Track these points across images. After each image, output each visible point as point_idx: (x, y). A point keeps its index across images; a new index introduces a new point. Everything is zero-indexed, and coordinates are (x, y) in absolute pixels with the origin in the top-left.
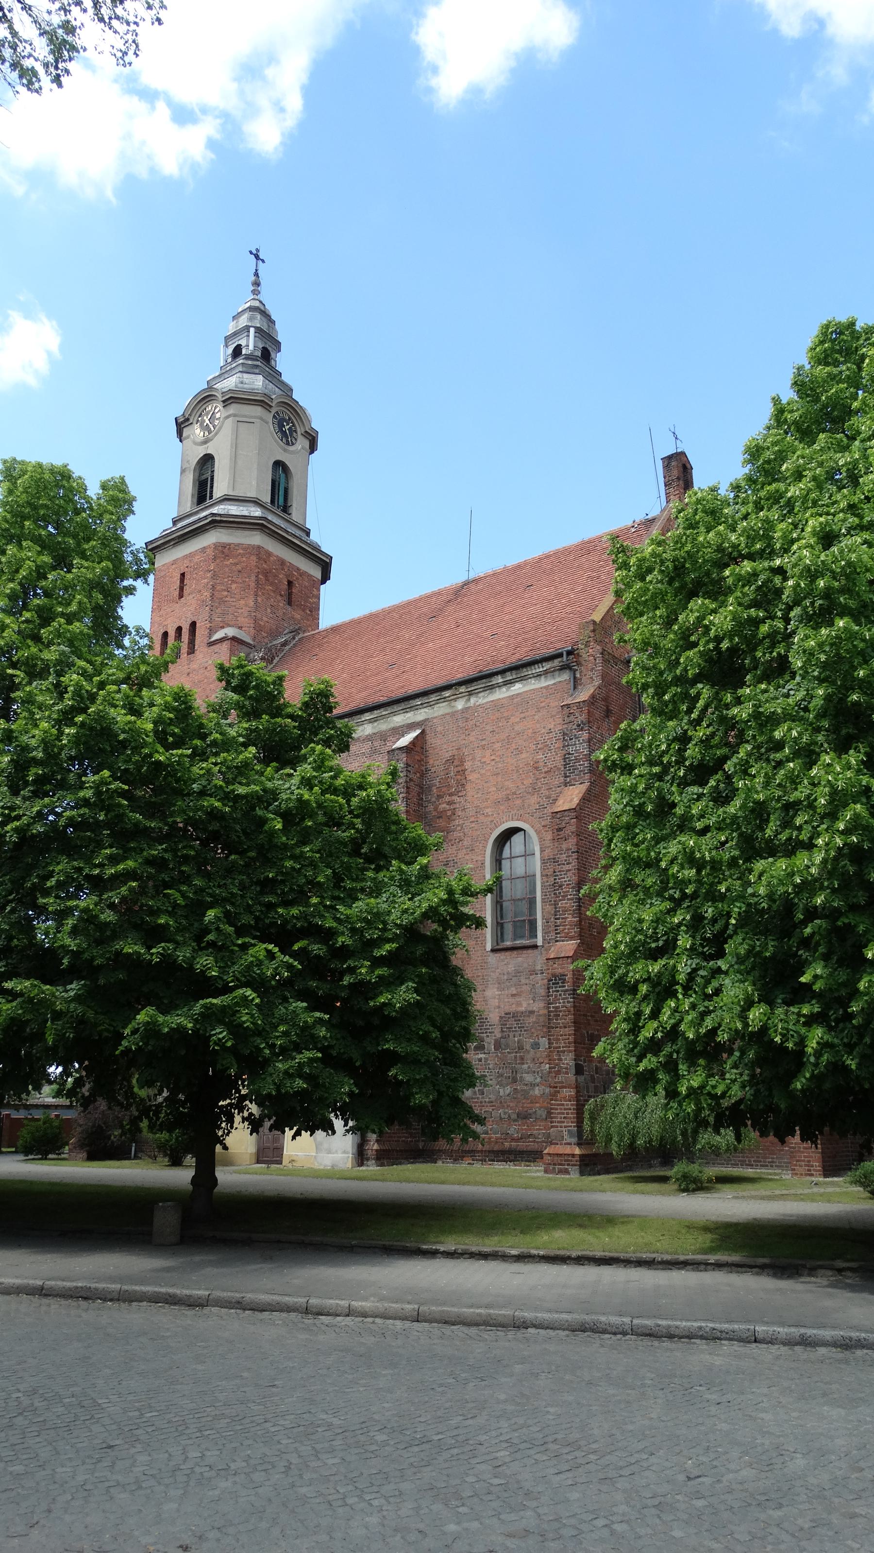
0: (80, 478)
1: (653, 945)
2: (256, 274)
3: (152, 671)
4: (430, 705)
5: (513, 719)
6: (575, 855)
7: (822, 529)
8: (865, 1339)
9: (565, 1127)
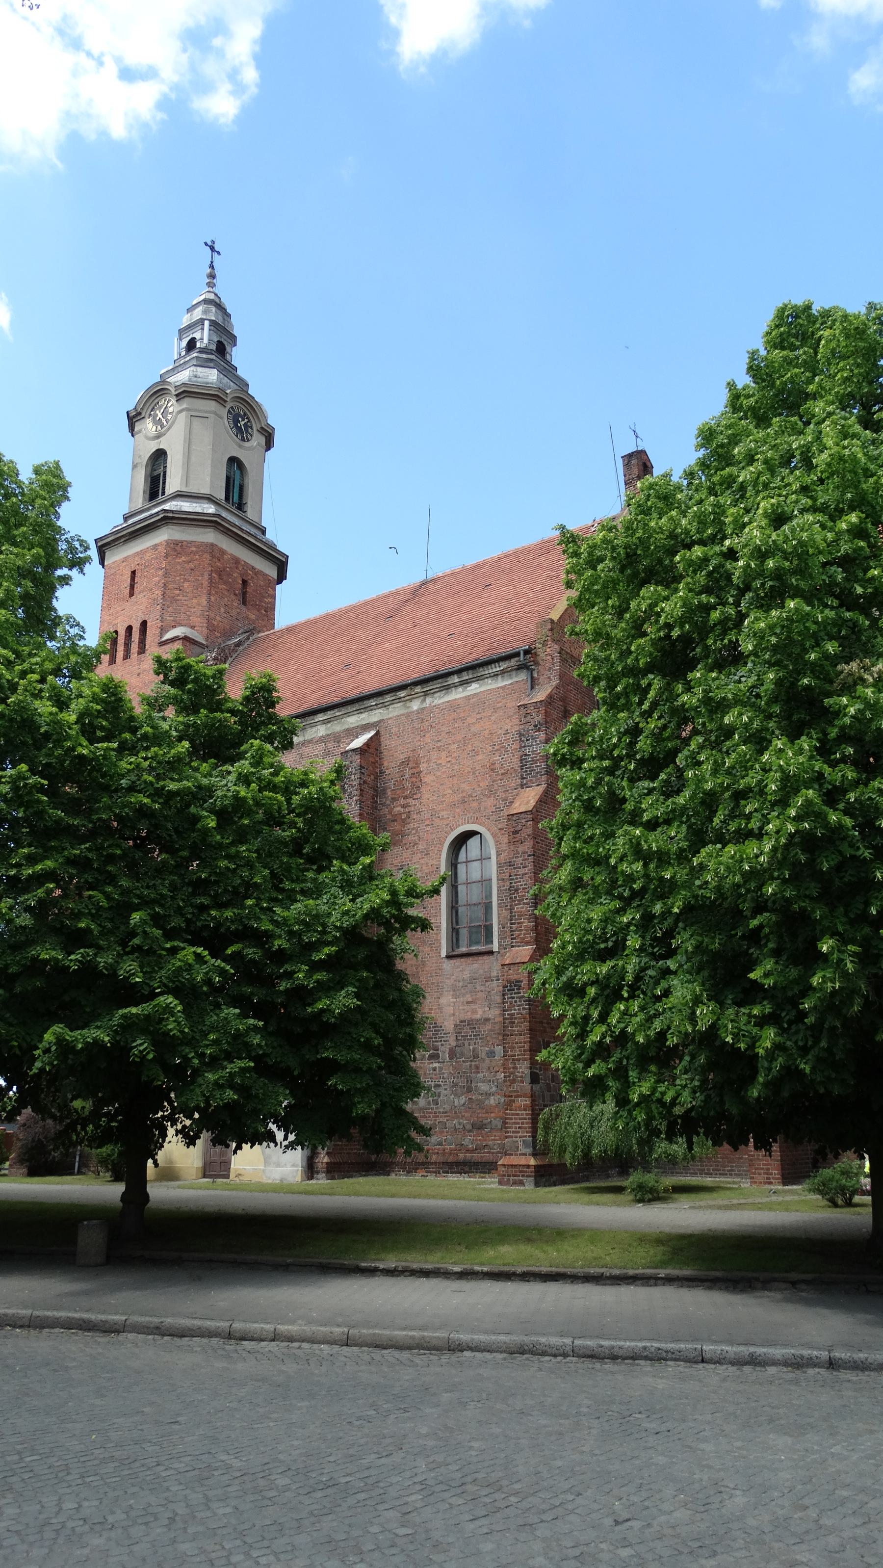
0: (12, 462)
1: (602, 946)
2: (212, 266)
3: (83, 662)
4: (384, 706)
5: (470, 720)
6: (531, 859)
7: (773, 511)
8: (817, 1357)
9: (520, 1137)
